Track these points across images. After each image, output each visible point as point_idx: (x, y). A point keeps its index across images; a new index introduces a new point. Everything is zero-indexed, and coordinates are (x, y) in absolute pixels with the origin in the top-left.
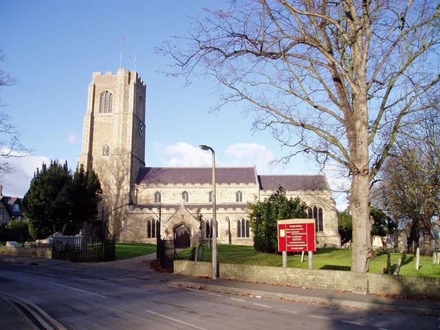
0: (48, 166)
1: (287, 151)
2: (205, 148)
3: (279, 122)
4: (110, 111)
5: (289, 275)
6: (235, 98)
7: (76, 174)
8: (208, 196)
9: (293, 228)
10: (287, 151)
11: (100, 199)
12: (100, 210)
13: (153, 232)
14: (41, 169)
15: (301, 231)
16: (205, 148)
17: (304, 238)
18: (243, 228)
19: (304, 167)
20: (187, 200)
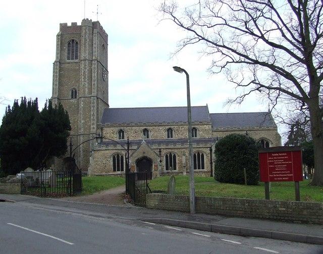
0: (19, 103)
1: (241, 91)
2: (178, 69)
3: (233, 62)
4: (76, 58)
5: (280, 209)
6: (193, 41)
7: (45, 110)
8: (166, 133)
9: (276, 156)
10: (241, 91)
11: (68, 135)
12: (68, 144)
13: (118, 166)
14: (12, 105)
15: (285, 160)
16: (178, 69)
17: (289, 167)
18: (118, 163)
19: (255, 104)
20: (148, 137)
